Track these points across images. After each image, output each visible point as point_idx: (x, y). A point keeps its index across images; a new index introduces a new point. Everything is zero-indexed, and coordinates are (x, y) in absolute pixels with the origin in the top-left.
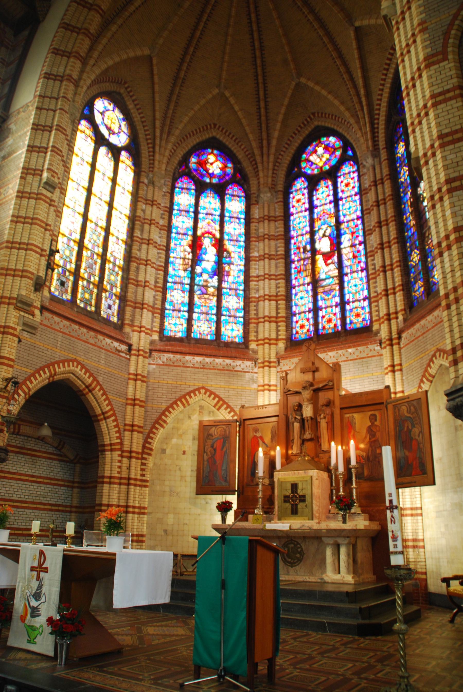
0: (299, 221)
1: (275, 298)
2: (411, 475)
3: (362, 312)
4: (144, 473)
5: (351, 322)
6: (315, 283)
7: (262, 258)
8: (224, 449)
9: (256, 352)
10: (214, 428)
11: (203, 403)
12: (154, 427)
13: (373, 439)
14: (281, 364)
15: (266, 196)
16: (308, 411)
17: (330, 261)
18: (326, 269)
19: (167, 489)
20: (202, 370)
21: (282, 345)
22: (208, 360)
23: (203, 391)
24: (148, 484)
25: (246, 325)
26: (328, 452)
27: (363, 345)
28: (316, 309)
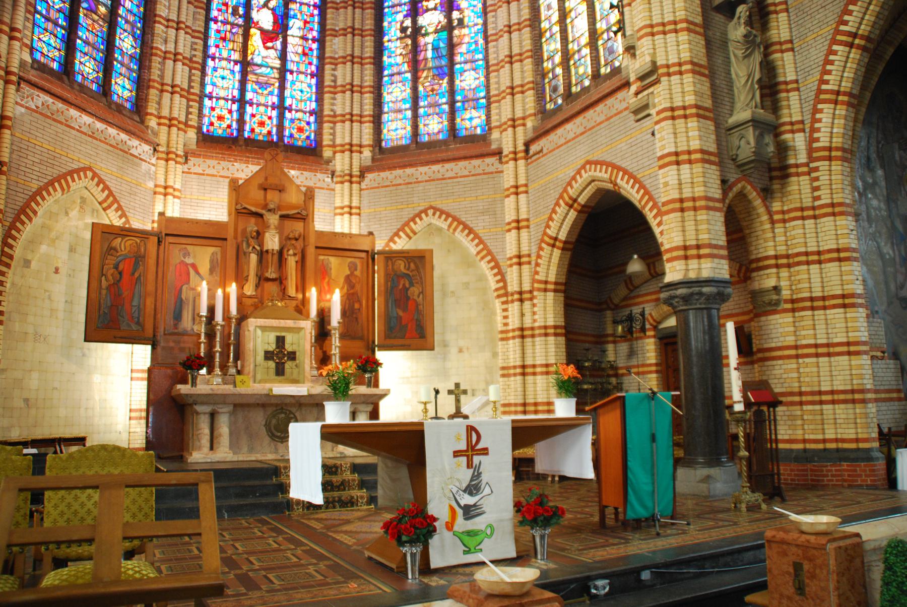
2: (403, 337)
3: (307, 127)
4: (505, 321)
5: (291, 136)
6: (245, 65)
8: (136, 275)
10: (119, 240)
11: (86, 194)
12: (17, 218)
13: (352, 291)
14: (191, 163)
17: (269, 44)
18: (264, 52)
19: (30, 330)
20: (90, 139)
21: (192, 134)
22: (99, 125)
23: (430, 212)
24: (500, 336)
27: (311, 170)
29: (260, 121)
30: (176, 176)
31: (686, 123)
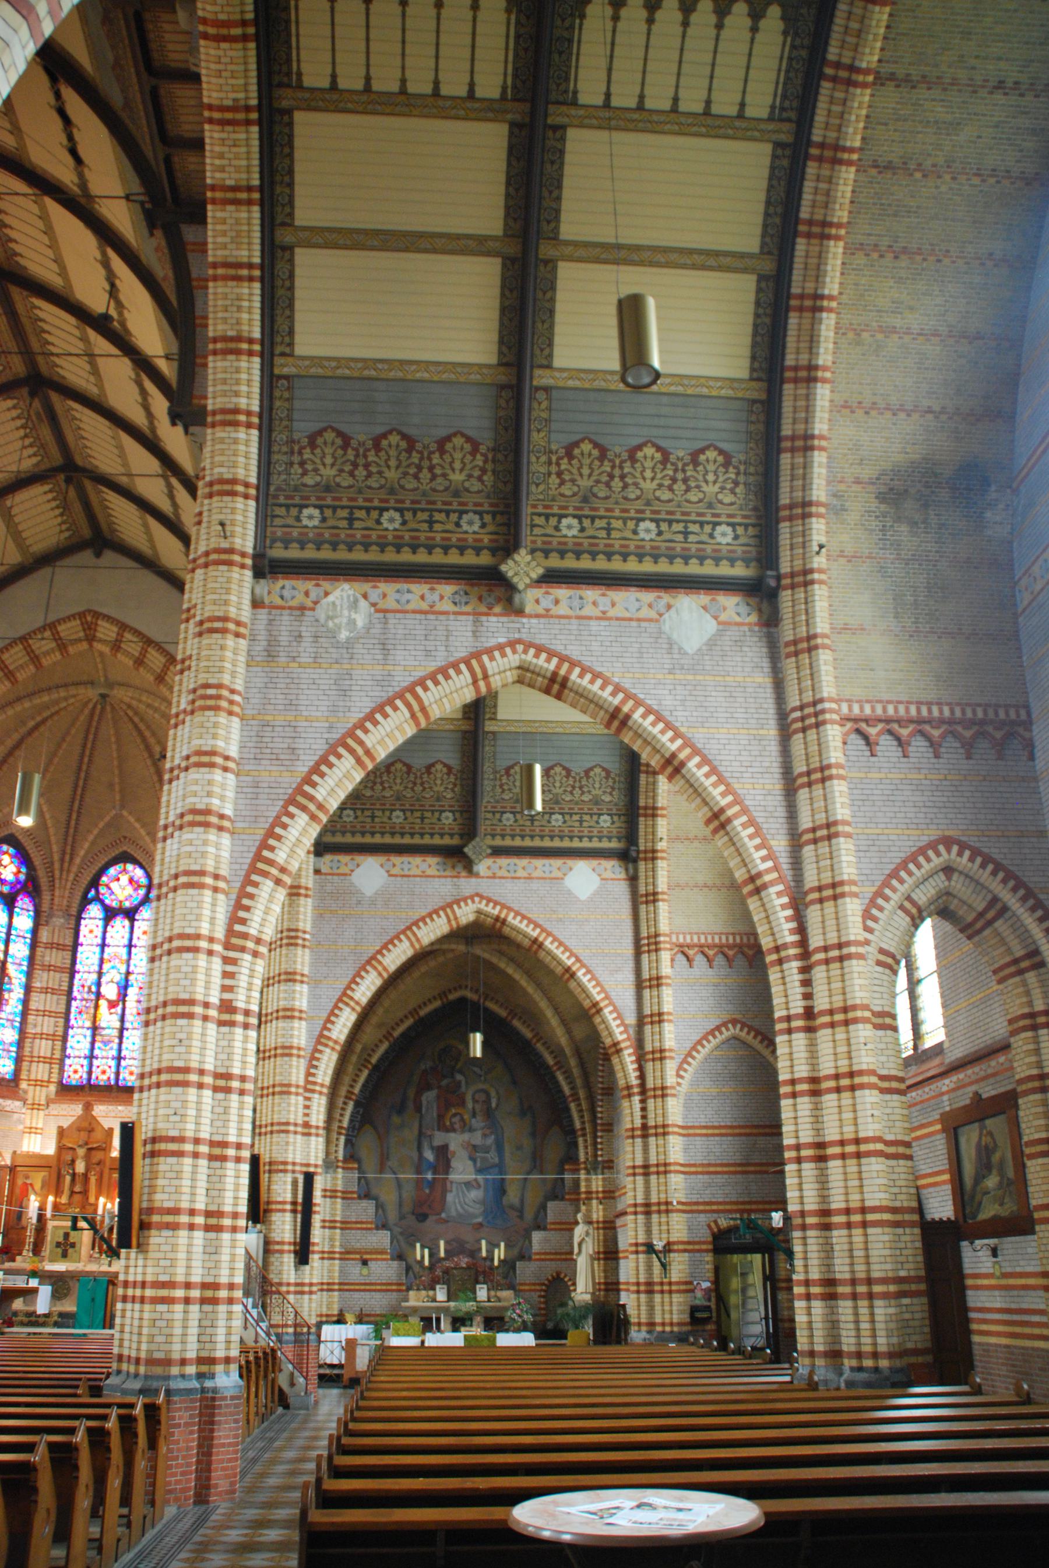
0: (87, 956)
1: (52, 1037)
6: (95, 1029)
7: (45, 990)
9: (26, 1092)
15: (58, 921)
16: (80, 1167)
21: (53, 1088)
25: (18, 1060)
26: (96, 1205)
28: (91, 1057)
29: (104, 1071)
30: (39, 1119)
31: (868, 1271)
